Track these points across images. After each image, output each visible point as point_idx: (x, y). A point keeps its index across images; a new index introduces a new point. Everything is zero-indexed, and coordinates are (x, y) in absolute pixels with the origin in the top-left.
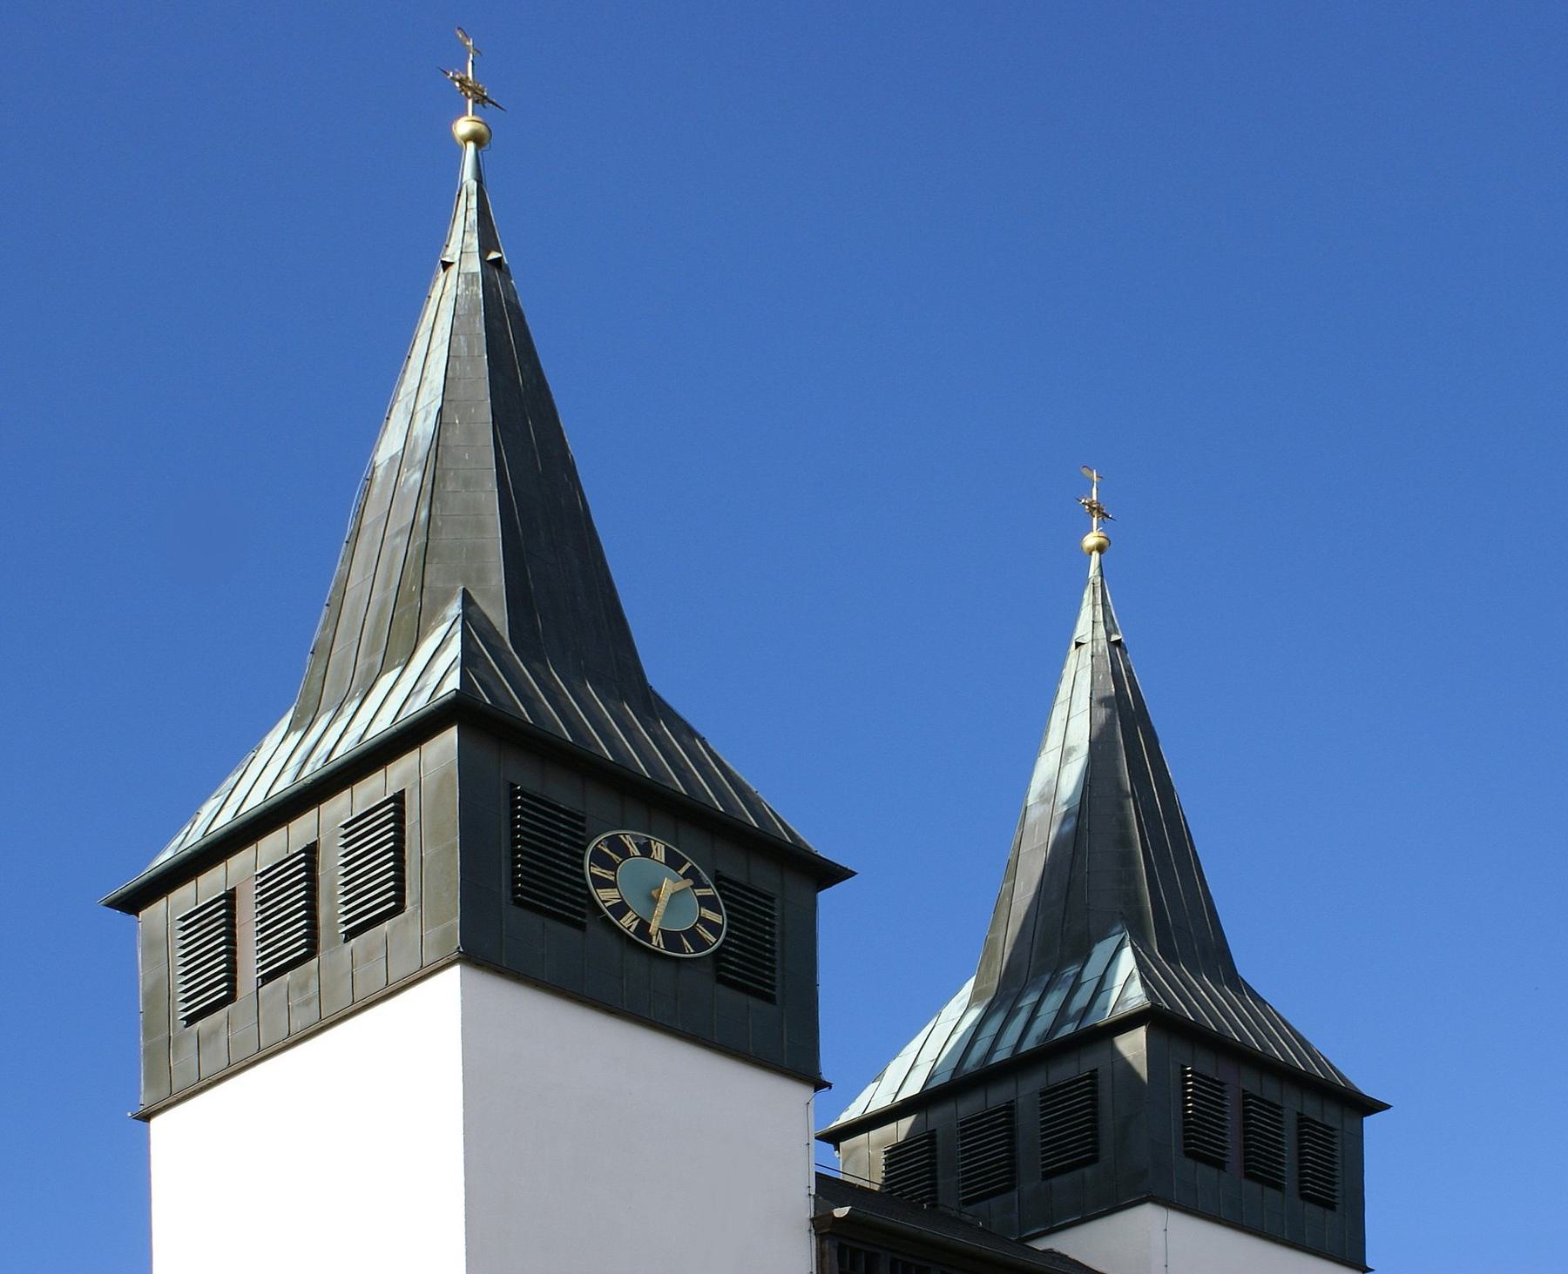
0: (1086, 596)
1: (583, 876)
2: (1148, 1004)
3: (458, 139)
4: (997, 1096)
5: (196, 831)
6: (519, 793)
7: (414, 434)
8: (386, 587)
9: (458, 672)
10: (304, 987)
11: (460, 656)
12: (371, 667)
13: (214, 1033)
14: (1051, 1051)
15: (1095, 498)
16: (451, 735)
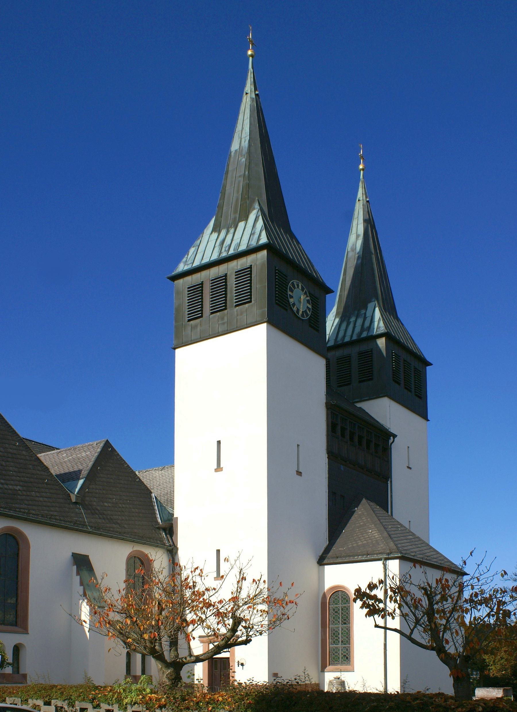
0: (360, 184)
1: (287, 295)
2: (386, 331)
3: (248, 55)
4: (346, 351)
5: (190, 258)
6: (277, 270)
7: (242, 145)
8: (238, 192)
9: (264, 231)
10: (223, 319)
11: (263, 225)
12: (235, 218)
13: (196, 326)
14: (360, 341)
15: (361, 153)
16: (265, 252)
